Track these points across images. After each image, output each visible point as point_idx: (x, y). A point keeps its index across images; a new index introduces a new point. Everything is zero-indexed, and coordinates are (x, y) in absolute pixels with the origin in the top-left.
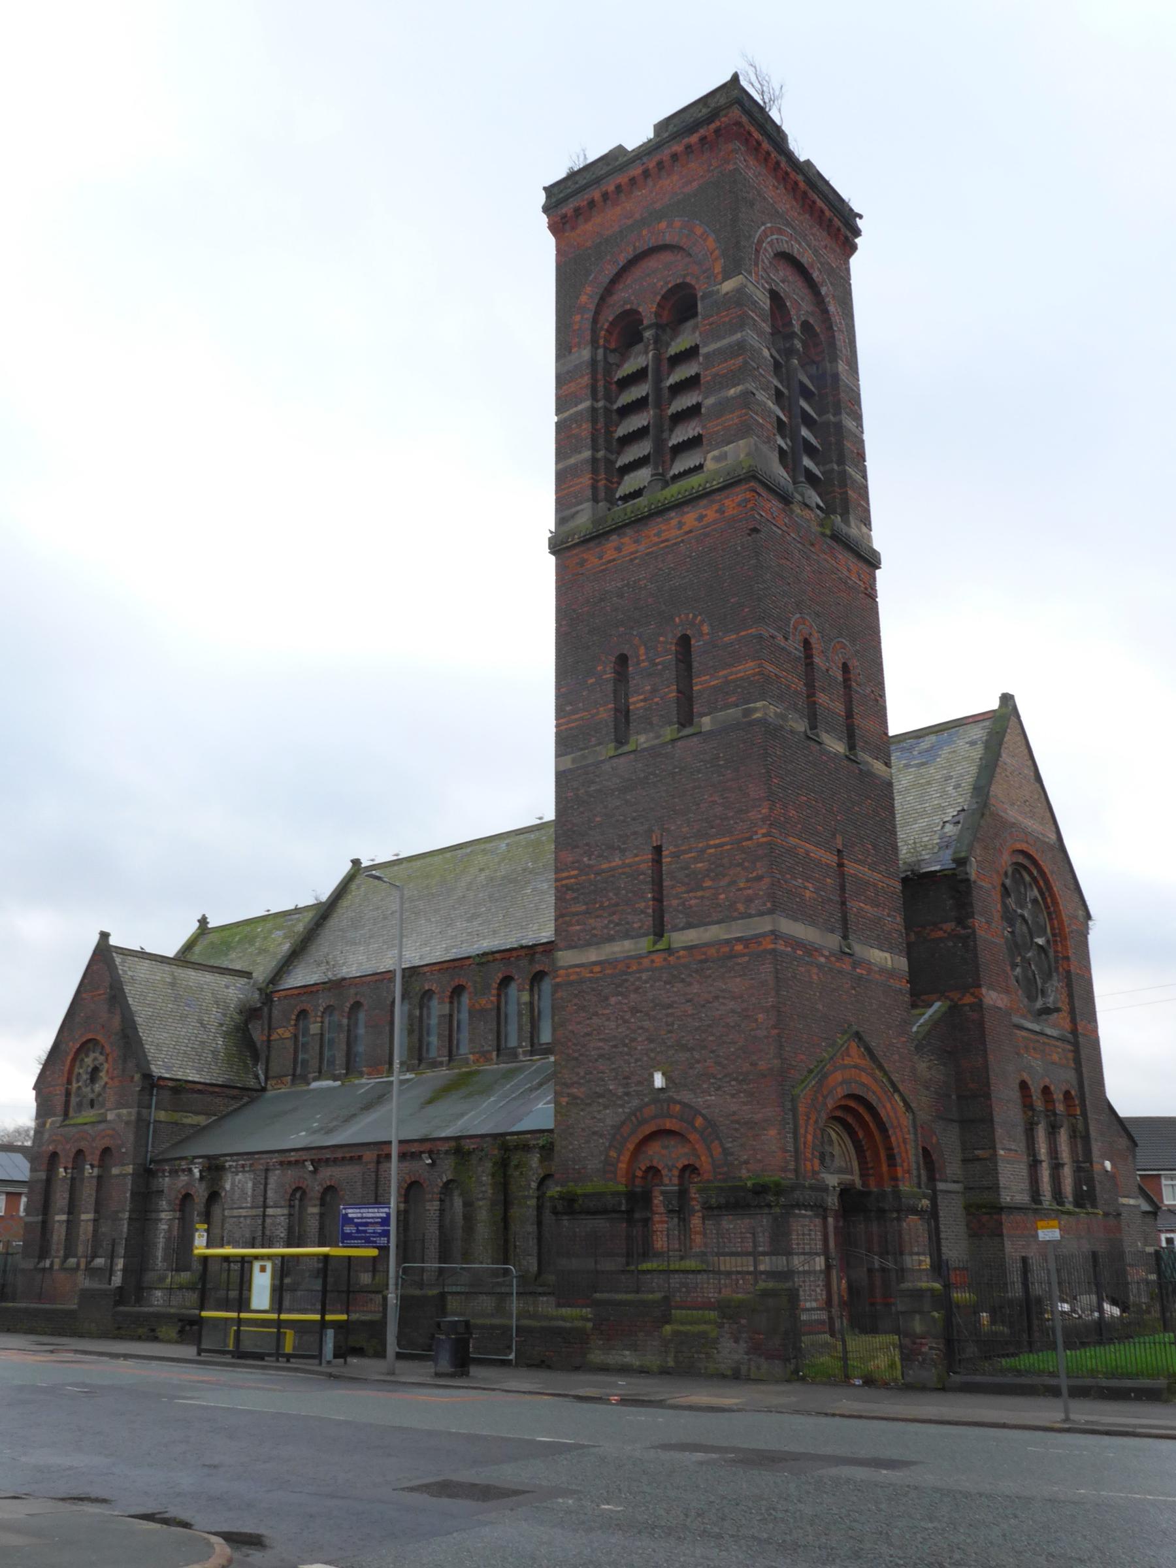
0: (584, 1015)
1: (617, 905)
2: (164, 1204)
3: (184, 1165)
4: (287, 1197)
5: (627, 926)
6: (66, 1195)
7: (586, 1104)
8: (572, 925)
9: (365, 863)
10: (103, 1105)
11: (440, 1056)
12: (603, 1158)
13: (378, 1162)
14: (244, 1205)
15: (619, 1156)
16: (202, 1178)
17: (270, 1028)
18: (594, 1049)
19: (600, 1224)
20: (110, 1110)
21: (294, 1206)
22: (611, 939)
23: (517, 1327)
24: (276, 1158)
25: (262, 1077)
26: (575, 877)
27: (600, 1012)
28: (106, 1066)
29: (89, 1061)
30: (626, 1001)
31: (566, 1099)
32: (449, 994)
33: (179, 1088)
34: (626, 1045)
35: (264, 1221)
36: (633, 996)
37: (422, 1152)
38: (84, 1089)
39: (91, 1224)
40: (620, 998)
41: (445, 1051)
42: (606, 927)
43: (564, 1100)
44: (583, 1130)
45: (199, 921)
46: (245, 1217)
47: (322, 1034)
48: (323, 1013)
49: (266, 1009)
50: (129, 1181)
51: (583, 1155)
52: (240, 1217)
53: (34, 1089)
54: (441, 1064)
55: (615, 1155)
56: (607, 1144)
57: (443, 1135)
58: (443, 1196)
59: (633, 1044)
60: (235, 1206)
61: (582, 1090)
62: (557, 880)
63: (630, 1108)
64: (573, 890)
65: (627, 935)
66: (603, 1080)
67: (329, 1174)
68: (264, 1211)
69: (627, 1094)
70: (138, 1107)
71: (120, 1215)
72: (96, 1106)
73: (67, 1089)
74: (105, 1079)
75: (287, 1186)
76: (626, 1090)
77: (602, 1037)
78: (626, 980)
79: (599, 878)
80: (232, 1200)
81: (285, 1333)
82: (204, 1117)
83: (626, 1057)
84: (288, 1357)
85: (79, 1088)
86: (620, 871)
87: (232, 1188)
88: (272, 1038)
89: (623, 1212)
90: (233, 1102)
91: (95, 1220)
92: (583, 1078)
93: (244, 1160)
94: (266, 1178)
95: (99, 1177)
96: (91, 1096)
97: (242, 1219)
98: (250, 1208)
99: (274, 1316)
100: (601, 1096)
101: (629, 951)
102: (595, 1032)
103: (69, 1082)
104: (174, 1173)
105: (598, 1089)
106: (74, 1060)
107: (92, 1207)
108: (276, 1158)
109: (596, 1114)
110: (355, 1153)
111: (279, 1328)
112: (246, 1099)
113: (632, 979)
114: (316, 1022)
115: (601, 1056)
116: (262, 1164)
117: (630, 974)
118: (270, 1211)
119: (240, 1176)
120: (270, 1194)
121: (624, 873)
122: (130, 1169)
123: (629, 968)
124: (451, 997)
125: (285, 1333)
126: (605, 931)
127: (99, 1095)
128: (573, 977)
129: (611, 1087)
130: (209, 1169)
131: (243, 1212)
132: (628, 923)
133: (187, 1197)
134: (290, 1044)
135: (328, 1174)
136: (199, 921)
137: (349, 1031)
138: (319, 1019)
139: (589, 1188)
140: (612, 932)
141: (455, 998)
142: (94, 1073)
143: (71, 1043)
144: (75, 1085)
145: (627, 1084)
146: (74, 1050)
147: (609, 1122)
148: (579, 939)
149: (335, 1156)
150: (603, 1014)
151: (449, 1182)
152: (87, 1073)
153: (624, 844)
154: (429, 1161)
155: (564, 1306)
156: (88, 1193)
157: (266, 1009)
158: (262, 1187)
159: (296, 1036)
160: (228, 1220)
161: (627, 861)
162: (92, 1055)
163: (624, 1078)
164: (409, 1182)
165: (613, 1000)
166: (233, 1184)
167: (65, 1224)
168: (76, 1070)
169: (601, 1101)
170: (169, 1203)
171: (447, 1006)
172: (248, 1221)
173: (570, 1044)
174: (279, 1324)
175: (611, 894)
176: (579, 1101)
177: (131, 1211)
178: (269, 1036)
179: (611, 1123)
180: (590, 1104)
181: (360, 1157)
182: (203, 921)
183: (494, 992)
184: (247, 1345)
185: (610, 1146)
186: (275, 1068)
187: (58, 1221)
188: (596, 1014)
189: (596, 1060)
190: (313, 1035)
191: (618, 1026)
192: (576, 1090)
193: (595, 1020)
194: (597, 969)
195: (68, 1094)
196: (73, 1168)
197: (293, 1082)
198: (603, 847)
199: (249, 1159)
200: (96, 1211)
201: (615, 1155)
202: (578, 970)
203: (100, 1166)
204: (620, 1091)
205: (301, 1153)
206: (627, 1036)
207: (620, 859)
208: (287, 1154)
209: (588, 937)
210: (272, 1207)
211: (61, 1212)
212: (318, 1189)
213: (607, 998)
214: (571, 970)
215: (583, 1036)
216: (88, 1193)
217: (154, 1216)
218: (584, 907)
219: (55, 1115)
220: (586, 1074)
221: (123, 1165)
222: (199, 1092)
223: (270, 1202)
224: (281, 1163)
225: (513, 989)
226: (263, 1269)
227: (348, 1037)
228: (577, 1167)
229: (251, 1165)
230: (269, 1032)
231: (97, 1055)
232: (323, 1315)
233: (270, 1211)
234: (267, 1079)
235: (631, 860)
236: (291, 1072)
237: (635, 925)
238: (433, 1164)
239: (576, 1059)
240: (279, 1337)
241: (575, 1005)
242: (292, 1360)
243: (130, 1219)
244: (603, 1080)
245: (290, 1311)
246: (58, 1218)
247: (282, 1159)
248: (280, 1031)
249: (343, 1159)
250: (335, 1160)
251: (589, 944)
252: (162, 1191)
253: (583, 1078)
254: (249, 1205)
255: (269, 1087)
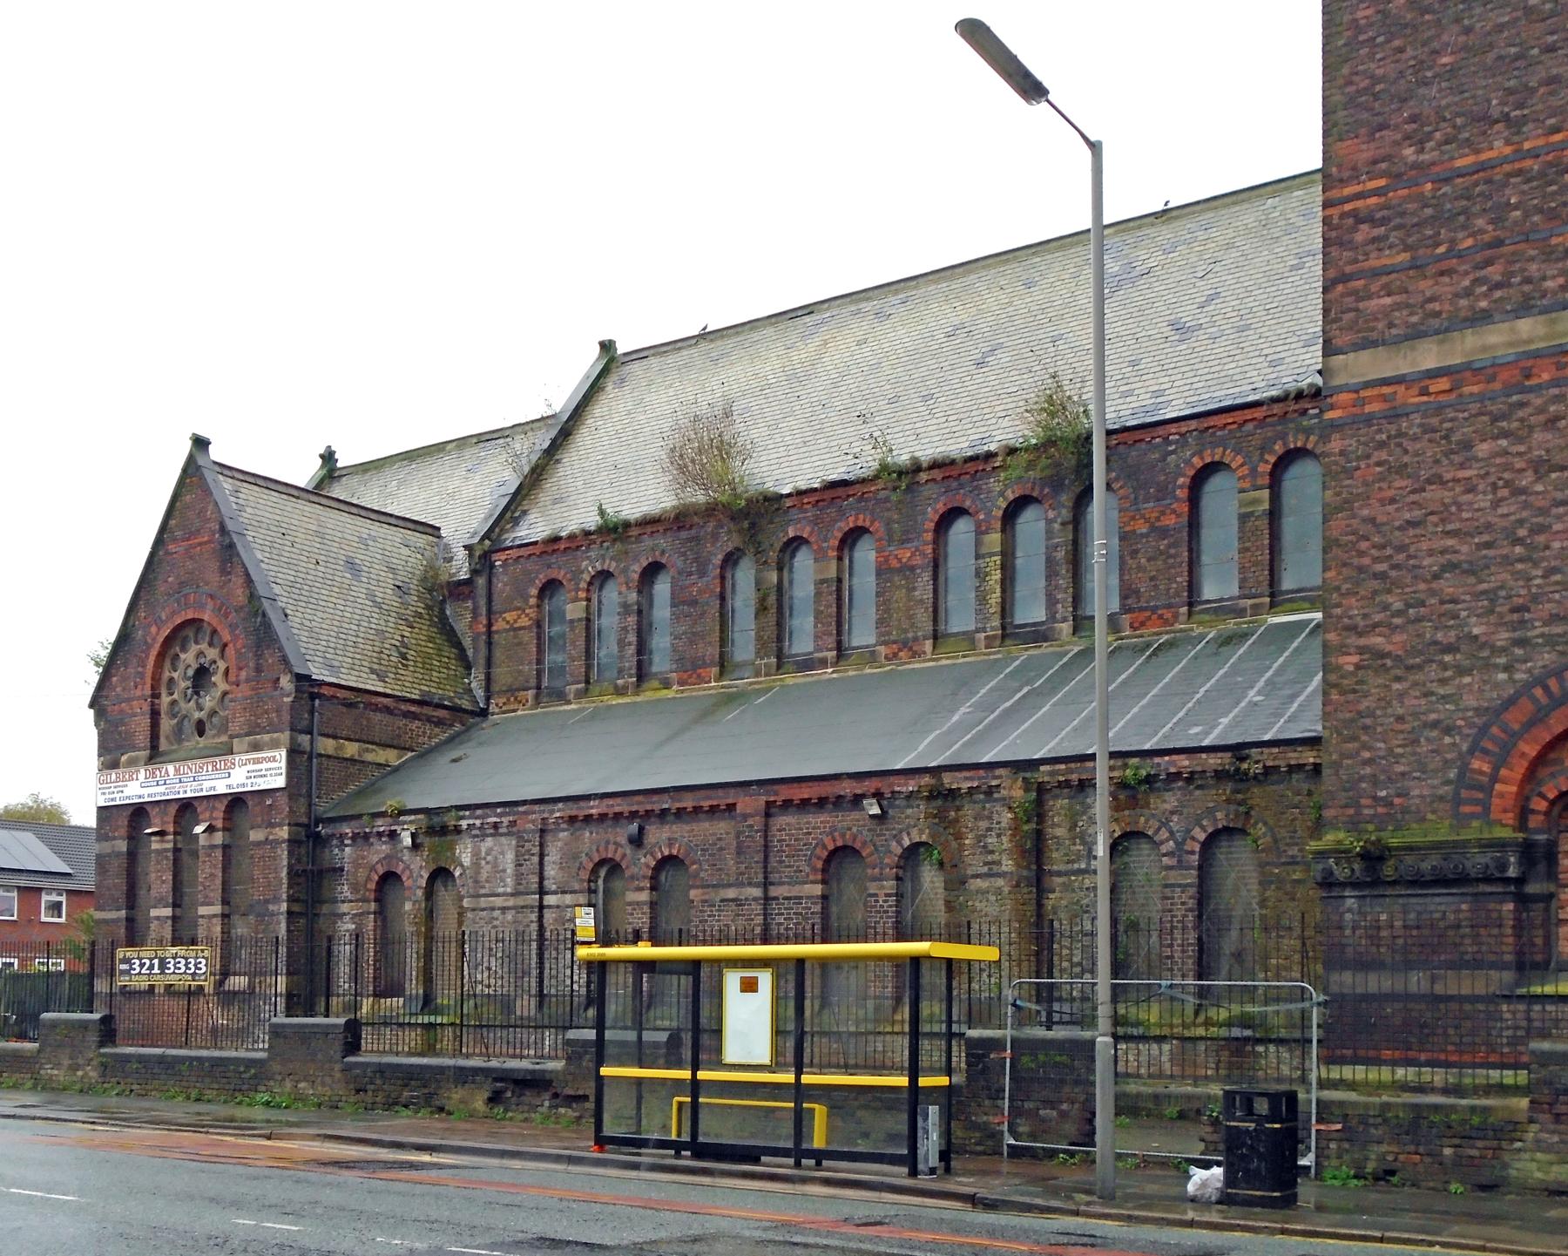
0: (1403, 483)
1: (1499, 243)
2: (345, 891)
3: (381, 825)
4: (585, 875)
5: (1527, 288)
6: (168, 877)
7: (1409, 668)
8: (1370, 297)
9: (621, 349)
10: (223, 728)
11: (820, 650)
12: (1452, 774)
13: (768, 815)
14: (501, 890)
15: (1496, 769)
16: (416, 846)
17: (490, 612)
18: (1431, 553)
19: (1446, 907)
20: (237, 736)
21: (595, 892)
22: (1480, 319)
23: (1319, 1102)
24: (559, 811)
25: (480, 693)
26: (1376, 192)
27: (1448, 476)
28: (222, 665)
29: (189, 658)
30: (1522, 449)
31: (1355, 659)
32: (837, 543)
33: (355, 699)
34: (1519, 541)
35: (541, 917)
36: (1538, 436)
37: (863, 796)
38: (182, 704)
39: (217, 922)
40: (1504, 443)
41: (831, 641)
42: (1468, 293)
43: (1349, 661)
44: (1400, 719)
45: (322, 456)
46: (504, 909)
47: (588, 620)
48: (590, 584)
49: (481, 581)
50: (283, 853)
51: (1400, 769)
52: (493, 909)
53: (91, 706)
54: (823, 663)
55: (1486, 768)
56: (1465, 747)
57: (898, 767)
58: (901, 872)
59: (1541, 539)
60: (483, 891)
61: (1397, 638)
62: (1326, 205)
63: (1529, 671)
64: (1371, 220)
65: (1524, 308)
66: (1456, 617)
67: (665, 836)
68: (541, 899)
69: (1522, 642)
70: (292, 730)
71: (271, 907)
72: (209, 732)
73: (153, 704)
74: (223, 686)
75: (584, 858)
76: (1517, 634)
77: (1449, 527)
78: (1522, 405)
79: (1446, 189)
80: (476, 882)
81: (813, 1110)
82: (395, 752)
83: (1519, 566)
84: (819, 1156)
85: (174, 702)
86: (1507, 168)
87: (476, 865)
88: (494, 628)
89: (1507, 881)
90: (437, 730)
91: (225, 916)
92: (1399, 613)
93: (499, 815)
94: (541, 845)
95: (226, 848)
96: (197, 715)
97: (497, 913)
98: (512, 895)
99: (789, 1078)
100: (1450, 649)
101: (1530, 341)
102: (1434, 518)
103: (156, 695)
104: (362, 838)
105: (1439, 636)
106: (161, 656)
107: (217, 895)
108: (559, 811)
109: (1434, 687)
110: (722, 799)
111: (798, 1102)
112: (458, 727)
113: (1539, 401)
114: (576, 600)
115: (1452, 567)
116: (533, 822)
117: (1531, 390)
118: (550, 900)
119: (489, 842)
120: (551, 871)
121: (1520, 172)
122: (284, 833)
123: (1528, 377)
124: (840, 548)
125: (813, 1110)
126: (1463, 302)
127: (213, 713)
128: (1374, 407)
129: (1476, 631)
130: (431, 831)
131: (498, 902)
132: (1528, 281)
133: (389, 879)
134: (529, 637)
135: (660, 837)
136: (322, 456)
137: (640, 612)
138: (582, 595)
139: (1414, 835)
140: (1483, 304)
141: (846, 552)
142: (201, 676)
143: (154, 629)
144: (165, 700)
145: (1522, 622)
146: (161, 639)
147: (1470, 701)
148: (1391, 325)
149: (678, 805)
150: (1456, 480)
151: (916, 846)
152: (185, 678)
153: (1521, 106)
154: (875, 810)
155: (1342, 1061)
156: (207, 872)
157: (481, 581)
158: (536, 859)
159: (539, 624)
160: (469, 915)
161: (1527, 146)
162: (194, 649)
163: (1514, 610)
164: (831, 847)
165: (1483, 449)
166: (476, 854)
167: (170, 922)
168: (166, 675)
169: (1448, 658)
170: (355, 888)
171: (834, 565)
172: (509, 916)
173: (1364, 545)
174: (799, 1092)
175: (1480, 222)
176: (1389, 662)
177: (292, 899)
178: (490, 625)
179: (1474, 703)
180: (1419, 667)
181: (731, 807)
182: (328, 457)
183: (929, 536)
184: (714, 1131)
185: (1471, 752)
186: (502, 674)
187: (158, 918)
188: (1437, 480)
189: (1436, 577)
190: (572, 621)
191: (1496, 504)
192: (1380, 640)
193: (1434, 494)
194: (1443, 384)
195: (155, 714)
196: (175, 833)
197: (538, 701)
198: (1459, 121)
199: (508, 814)
200: (225, 902)
201: (1486, 768)
202: (1386, 390)
203: (225, 829)
204: (1503, 637)
205: (611, 802)
206: (1521, 522)
207: (1508, 142)
208: (582, 804)
209: (1414, 319)
210: (555, 893)
211: (160, 903)
212: (647, 861)
213: (1467, 445)
214: (1363, 394)
215: (1400, 528)
216: (207, 872)
217: (325, 909)
218: (1404, 257)
219: (134, 748)
220: (1408, 606)
221: (271, 825)
222: (388, 710)
223: (550, 885)
224: (572, 820)
225: (961, 530)
226: (749, 986)
227: (639, 623)
228: (1383, 793)
229: (513, 824)
230: (489, 620)
231: (204, 646)
232: (799, 1074)
233: (550, 900)
234: (488, 699)
235: (1540, 142)
236: (533, 682)
237: (1549, 284)
238: (880, 818)
239: (1382, 576)
240: (800, 1121)
241: (1379, 464)
242: (825, 1163)
243: (290, 913)
244: (1456, 617)
245: (823, 1068)
246: (154, 913)
247: (574, 813)
248: (509, 616)
249: (697, 810)
250: (680, 813)
251: (1415, 334)
252: (342, 869)
253: (1399, 613)
254: (509, 890)
255: (492, 708)
